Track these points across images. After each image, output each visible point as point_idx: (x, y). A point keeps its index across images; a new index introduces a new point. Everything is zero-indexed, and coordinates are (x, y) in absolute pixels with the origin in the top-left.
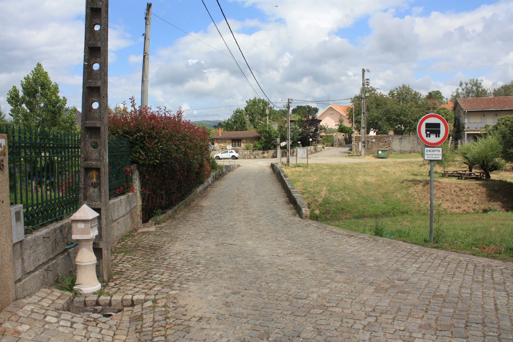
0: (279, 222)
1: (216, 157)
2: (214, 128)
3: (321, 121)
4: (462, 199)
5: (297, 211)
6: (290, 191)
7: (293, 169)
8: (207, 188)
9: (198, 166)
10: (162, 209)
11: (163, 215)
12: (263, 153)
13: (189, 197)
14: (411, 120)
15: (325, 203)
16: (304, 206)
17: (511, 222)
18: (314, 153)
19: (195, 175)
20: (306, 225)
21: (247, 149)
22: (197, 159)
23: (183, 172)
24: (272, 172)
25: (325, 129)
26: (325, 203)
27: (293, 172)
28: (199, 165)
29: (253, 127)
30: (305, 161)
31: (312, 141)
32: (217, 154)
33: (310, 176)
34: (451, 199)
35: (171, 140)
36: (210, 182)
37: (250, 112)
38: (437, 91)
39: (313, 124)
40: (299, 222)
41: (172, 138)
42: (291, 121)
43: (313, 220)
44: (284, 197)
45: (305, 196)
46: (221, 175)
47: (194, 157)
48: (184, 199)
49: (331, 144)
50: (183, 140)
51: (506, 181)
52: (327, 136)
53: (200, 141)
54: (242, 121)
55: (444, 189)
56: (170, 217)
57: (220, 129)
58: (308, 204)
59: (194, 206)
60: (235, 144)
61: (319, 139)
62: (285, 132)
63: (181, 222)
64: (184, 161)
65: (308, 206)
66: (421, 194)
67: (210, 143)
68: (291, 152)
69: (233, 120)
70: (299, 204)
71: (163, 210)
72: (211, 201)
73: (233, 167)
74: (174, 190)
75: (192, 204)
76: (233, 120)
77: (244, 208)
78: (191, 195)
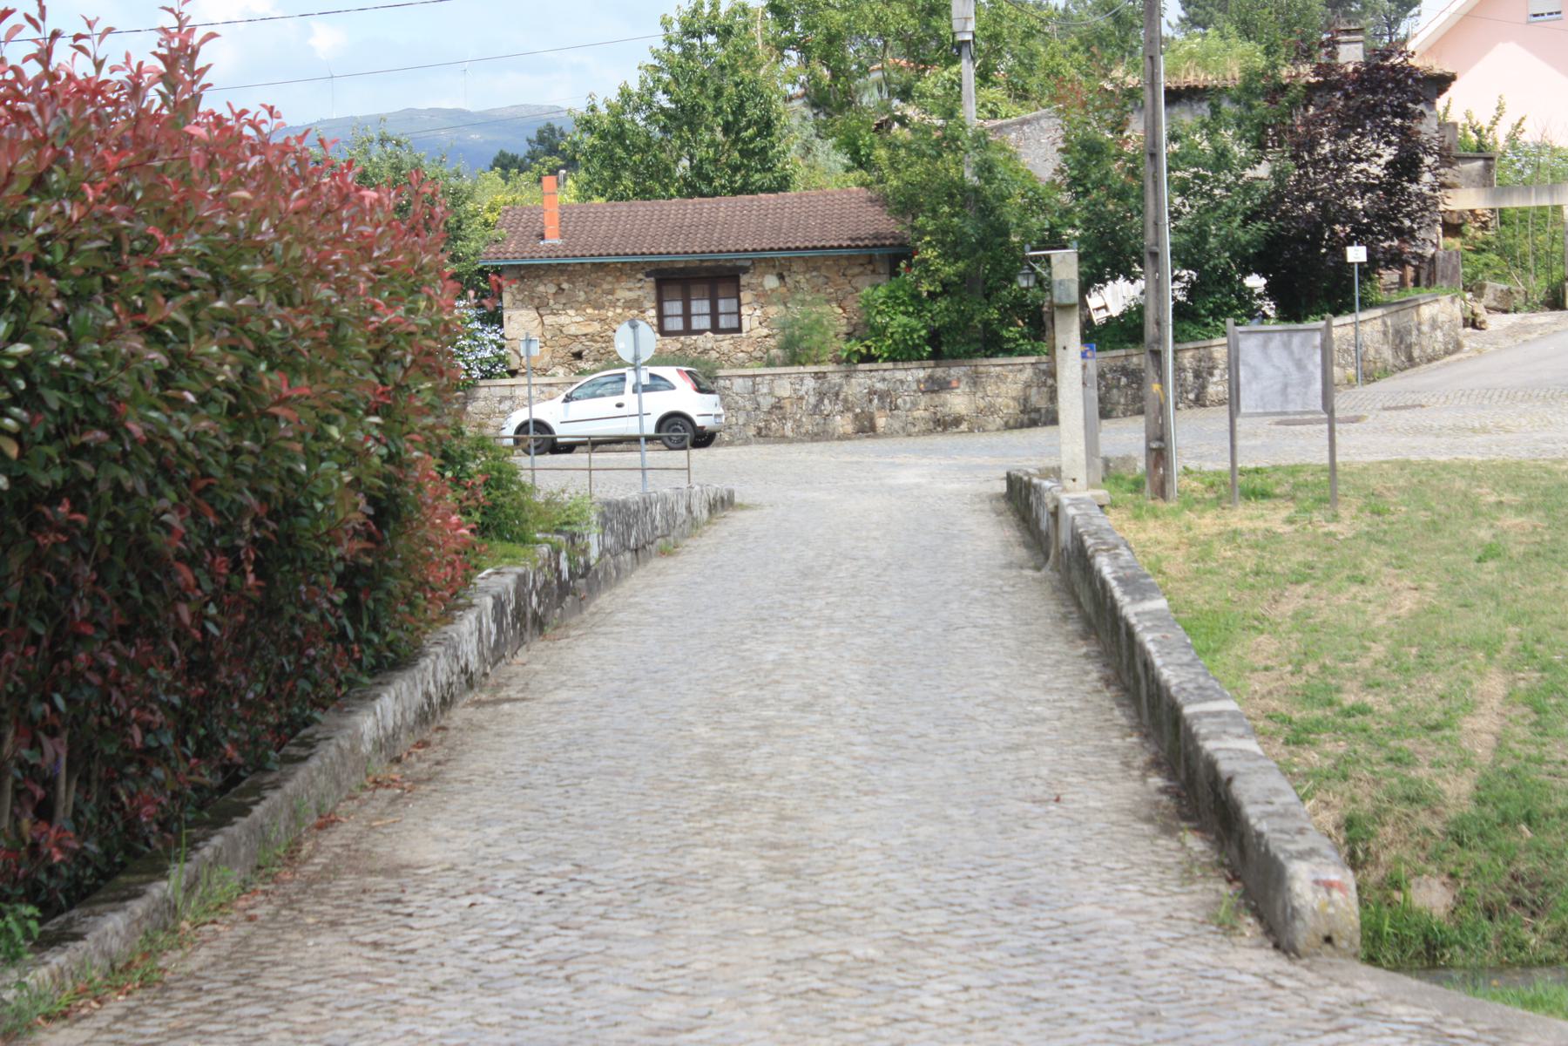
0: (1082, 990)
1: (523, 428)
2: (495, 175)
3: (1442, 82)
5: (1246, 894)
6: (1175, 709)
7: (1207, 523)
8: (447, 703)
9: (356, 511)
10: (43, 907)
11: (58, 959)
12: (937, 386)
13: (289, 787)
15: (1505, 819)
16: (1303, 844)
17: (8, 890)
18: (1386, 372)
19: (340, 597)
20: (1329, 1013)
21: (794, 352)
22: (352, 455)
23: (222, 564)
24: (1021, 553)
25: (1483, 153)
26: (1505, 819)
27: (1202, 549)
28: (372, 501)
29: (844, 159)
30: (1307, 447)
31: (1368, 270)
32: (530, 401)
33: (1352, 579)
35: (108, 285)
36: (470, 651)
37: (808, 27)
39: (1373, 111)
40: (1265, 989)
41: (120, 268)
42: (1175, 96)
43: (1397, 968)
44: (1127, 764)
45: (1313, 756)
46: (564, 589)
47: (320, 436)
48: (244, 811)
49: (1539, 286)
50: (217, 287)
52: (1503, 218)
53: (376, 288)
54: (740, 110)
56: (119, 973)
57: (549, 181)
58: (1350, 823)
59: (331, 872)
60: (687, 316)
61: (1433, 242)
62: (1121, 195)
63: (216, 1011)
64: (236, 473)
65: (1351, 841)
67: (465, 308)
68: (1179, 369)
69: (663, 100)
70: (1263, 826)
71: (49, 910)
72: (481, 822)
73: (670, 514)
74: (147, 729)
75: (317, 848)
76: (663, 100)
77: (774, 873)
78: (302, 773)
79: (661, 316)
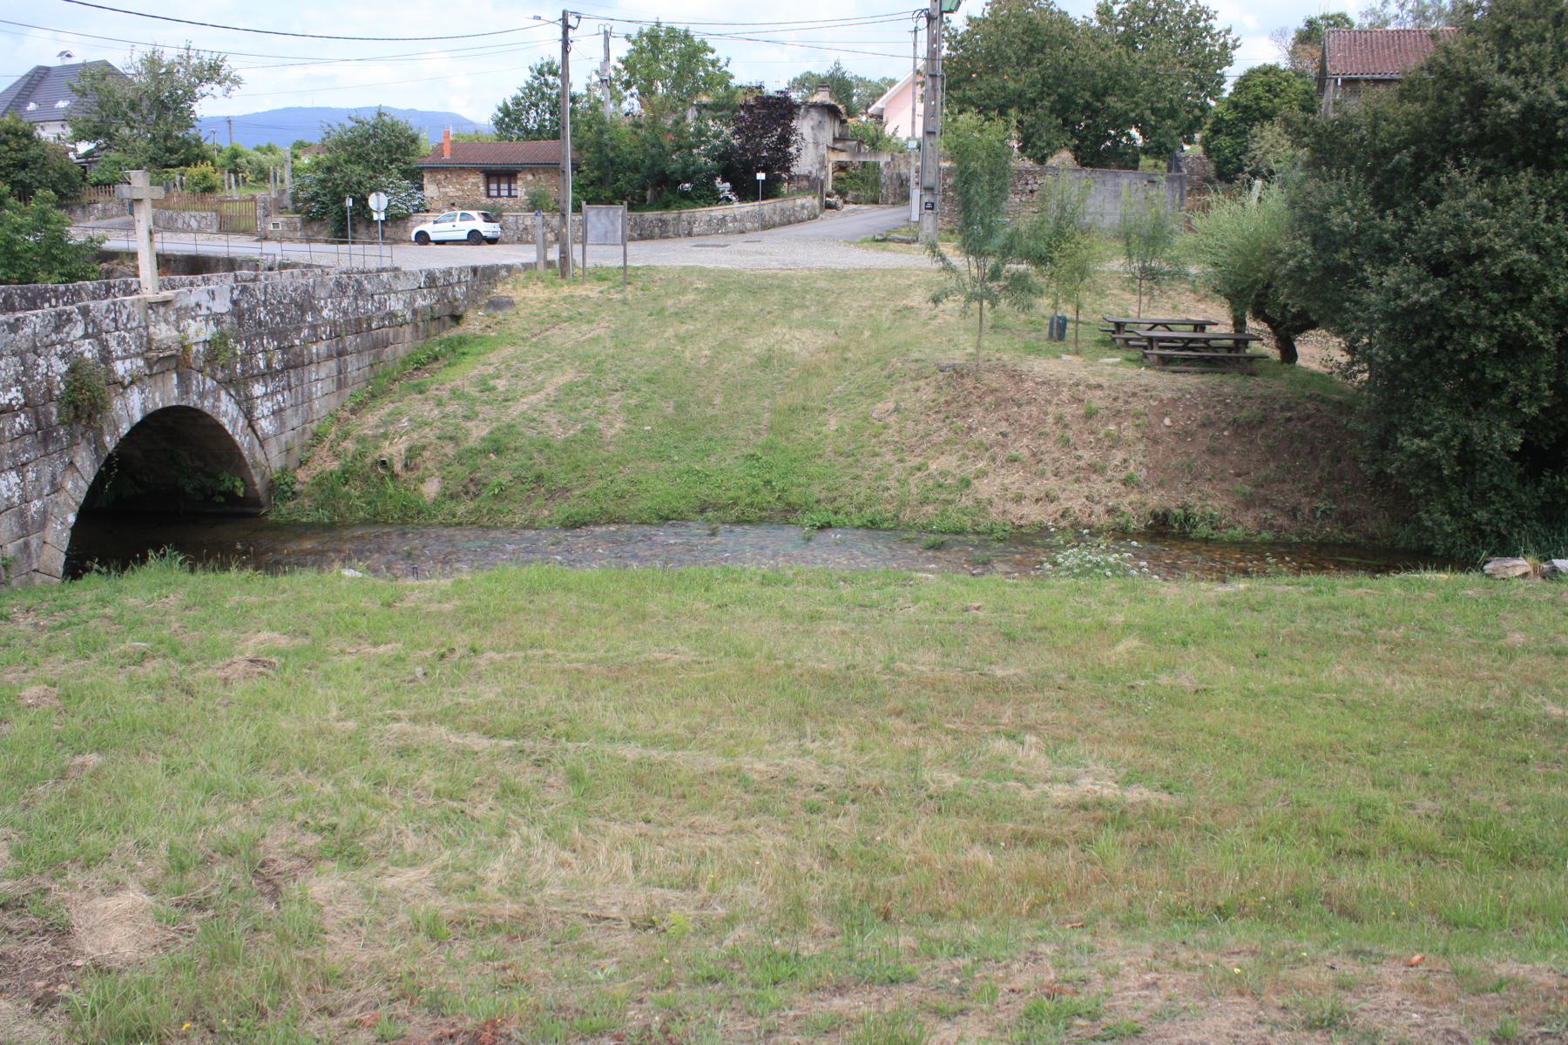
4: (1079, 458)
14: (1148, 112)
34: (1034, 455)
38: (1339, 15)
51: (75, 529)
55: (1019, 406)
60: (499, 190)
66: (917, 422)
79: (488, 190)
